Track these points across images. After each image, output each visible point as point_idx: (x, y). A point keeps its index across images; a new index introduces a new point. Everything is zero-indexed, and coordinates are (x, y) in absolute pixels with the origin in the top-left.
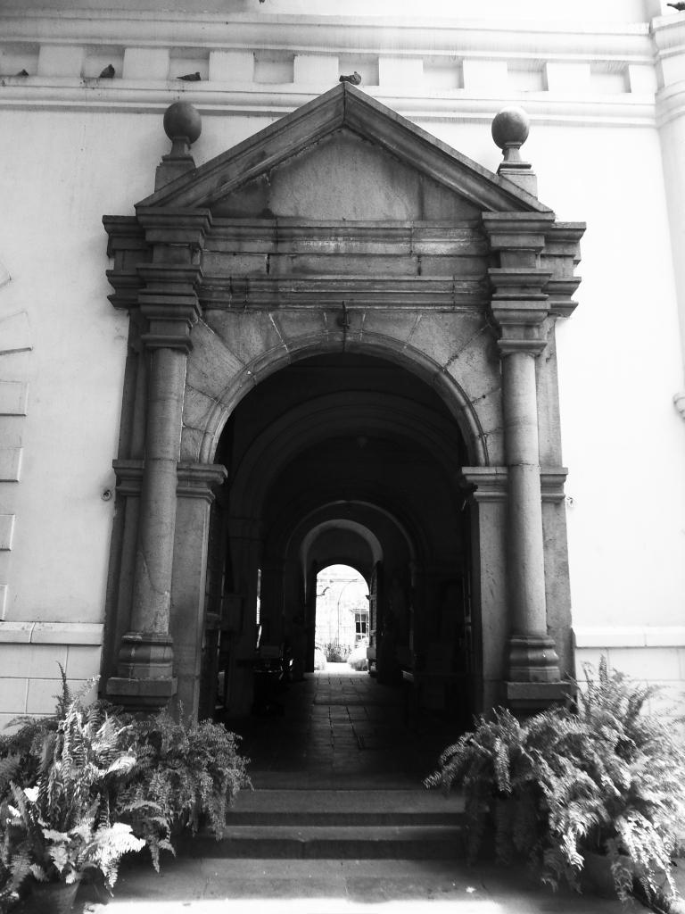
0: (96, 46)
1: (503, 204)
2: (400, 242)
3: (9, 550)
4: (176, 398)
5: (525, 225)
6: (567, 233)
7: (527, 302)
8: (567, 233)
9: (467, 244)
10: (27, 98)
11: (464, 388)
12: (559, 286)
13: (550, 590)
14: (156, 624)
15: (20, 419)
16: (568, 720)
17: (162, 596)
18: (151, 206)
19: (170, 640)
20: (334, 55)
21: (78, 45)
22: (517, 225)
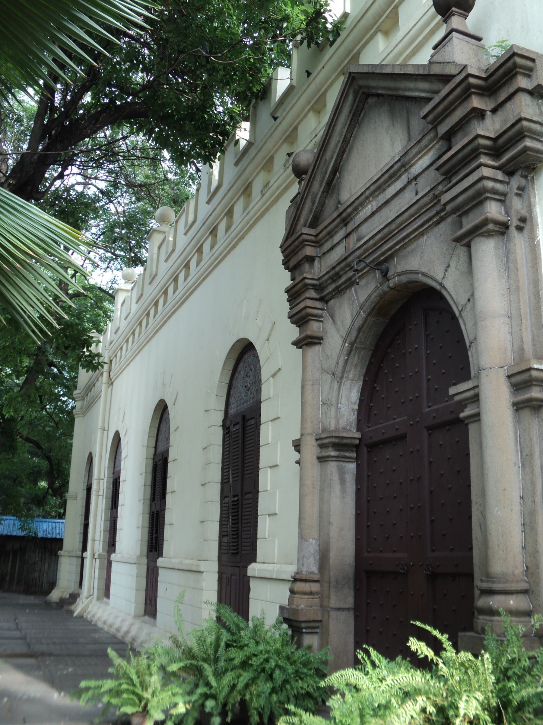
0: (288, 136)
1: (435, 86)
2: (401, 175)
3: (276, 514)
4: (311, 382)
5: (451, 97)
6: (501, 71)
7: (465, 180)
8: (501, 71)
9: (440, 143)
10: (272, 196)
11: (455, 297)
12: (506, 137)
13: (527, 521)
14: (303, 565)
15: (278, 420)
16: (432, 677)
17: (307, 543)
18: (285, 242)
19: (316, 577)
20: (375, 33)
21: (282, 143)
22: (446, 102)
